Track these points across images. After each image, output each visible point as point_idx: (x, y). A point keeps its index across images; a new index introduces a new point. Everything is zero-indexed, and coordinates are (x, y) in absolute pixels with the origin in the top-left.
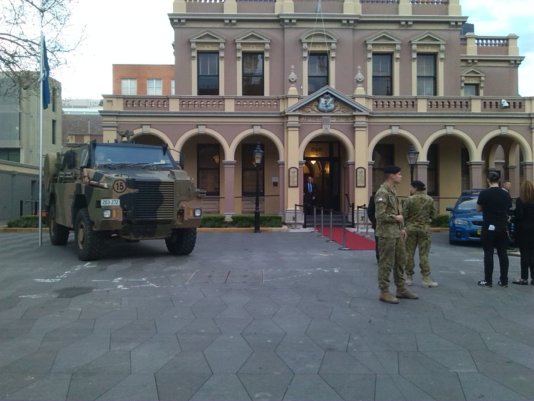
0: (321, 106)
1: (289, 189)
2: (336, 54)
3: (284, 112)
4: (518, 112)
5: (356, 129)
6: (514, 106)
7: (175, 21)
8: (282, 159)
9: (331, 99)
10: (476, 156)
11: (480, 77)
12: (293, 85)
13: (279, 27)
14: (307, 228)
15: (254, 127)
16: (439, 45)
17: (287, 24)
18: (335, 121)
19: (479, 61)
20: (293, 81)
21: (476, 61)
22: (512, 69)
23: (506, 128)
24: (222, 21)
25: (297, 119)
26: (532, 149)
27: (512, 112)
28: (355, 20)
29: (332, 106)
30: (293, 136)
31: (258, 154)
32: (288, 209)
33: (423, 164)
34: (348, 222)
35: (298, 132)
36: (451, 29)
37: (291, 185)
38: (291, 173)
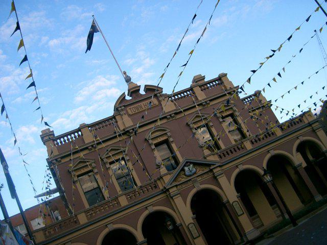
0: (187, 173)
3: (165, 188)
5: (174, 198)
9: (191, 165)
18: (200, 179)
26: (322, 142)
28: (174, 113)
29: (195, 170)
38: (190, 229)
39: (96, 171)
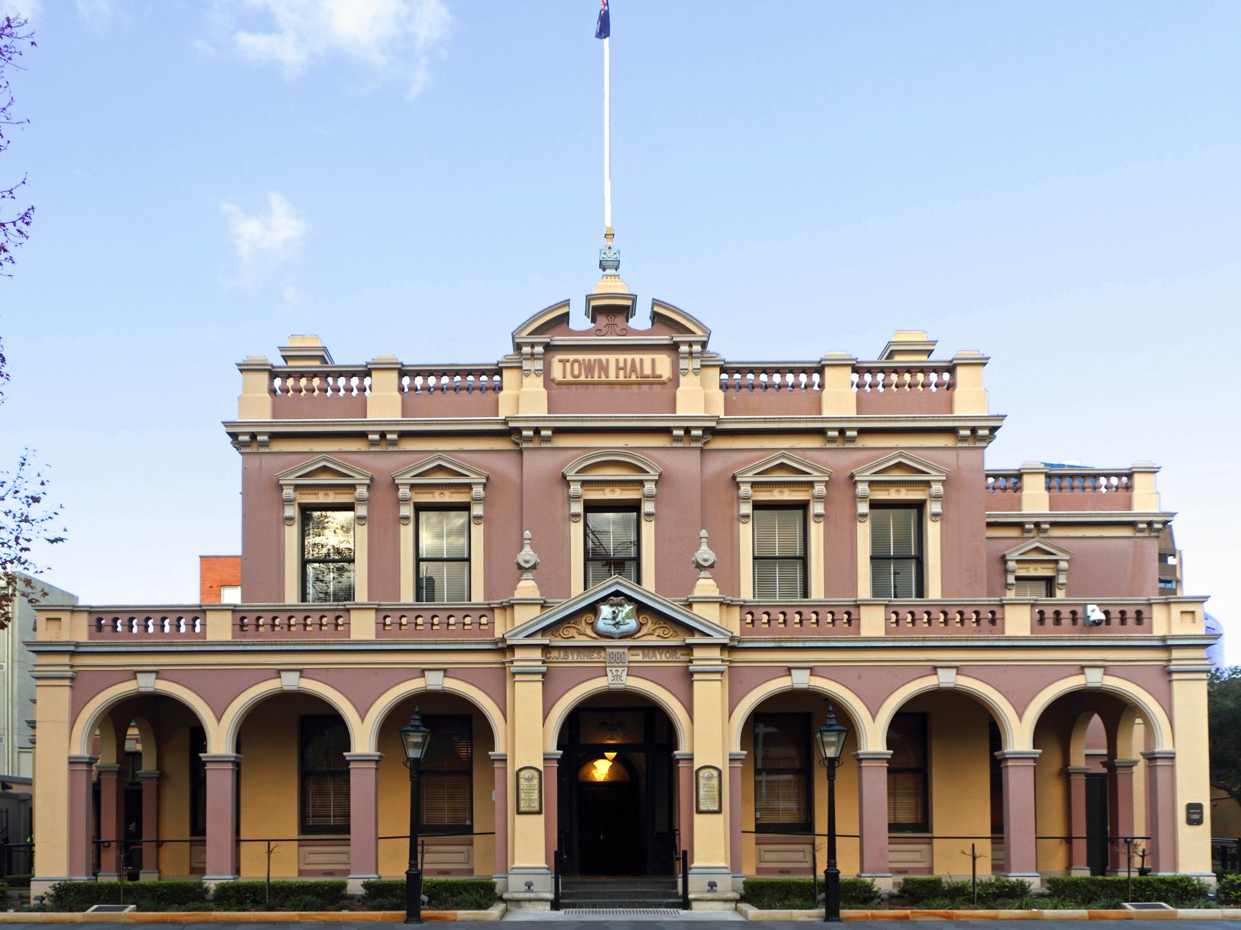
0: (601, 625)
1: (519, 818)
2: (656, 507)
4: (1133, 634)
5: (696, 677)
6: (1123, 621)
7: (241, 438)
8: (500, 748)
9: (628, 608)
10: (1019, 737)
11: (1056, 562)
12: (530, 575)
13: (512, 447)
14: (562, 912)
15: (426, 673)
16: (927, 484)
17: (529, 439)
18: (639, 658)
19: (1054, 525)
20: (527, 566)
21: (1047, 526)
22: (1140, 541)
23: (1100, 672)
24: (363, 435)
25: (538, 654)
27: (1116, 634)
30: (528, 694)
31: (444, 740)
32: (516, 865)
33: (874, 758)
34: (676, 895)
35: (540, 684)
36: (960, 445)
37: (522, 809)
38: (522, 781)
39: (477, 510)
